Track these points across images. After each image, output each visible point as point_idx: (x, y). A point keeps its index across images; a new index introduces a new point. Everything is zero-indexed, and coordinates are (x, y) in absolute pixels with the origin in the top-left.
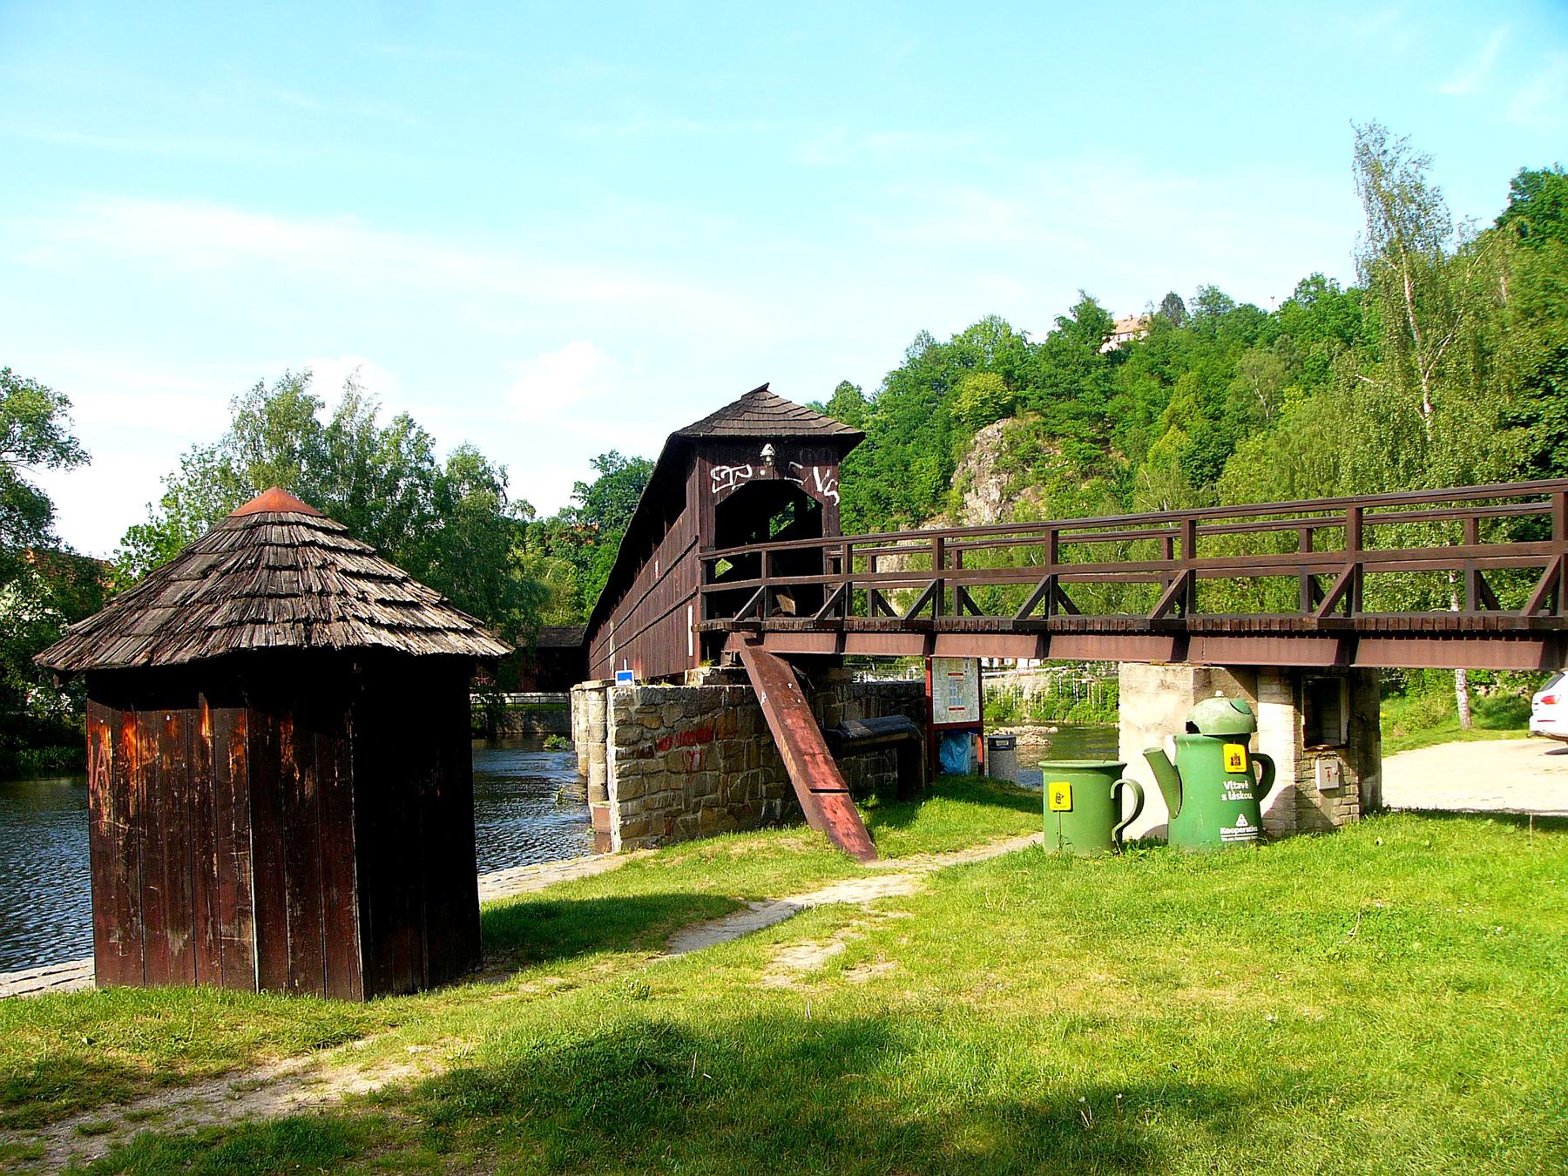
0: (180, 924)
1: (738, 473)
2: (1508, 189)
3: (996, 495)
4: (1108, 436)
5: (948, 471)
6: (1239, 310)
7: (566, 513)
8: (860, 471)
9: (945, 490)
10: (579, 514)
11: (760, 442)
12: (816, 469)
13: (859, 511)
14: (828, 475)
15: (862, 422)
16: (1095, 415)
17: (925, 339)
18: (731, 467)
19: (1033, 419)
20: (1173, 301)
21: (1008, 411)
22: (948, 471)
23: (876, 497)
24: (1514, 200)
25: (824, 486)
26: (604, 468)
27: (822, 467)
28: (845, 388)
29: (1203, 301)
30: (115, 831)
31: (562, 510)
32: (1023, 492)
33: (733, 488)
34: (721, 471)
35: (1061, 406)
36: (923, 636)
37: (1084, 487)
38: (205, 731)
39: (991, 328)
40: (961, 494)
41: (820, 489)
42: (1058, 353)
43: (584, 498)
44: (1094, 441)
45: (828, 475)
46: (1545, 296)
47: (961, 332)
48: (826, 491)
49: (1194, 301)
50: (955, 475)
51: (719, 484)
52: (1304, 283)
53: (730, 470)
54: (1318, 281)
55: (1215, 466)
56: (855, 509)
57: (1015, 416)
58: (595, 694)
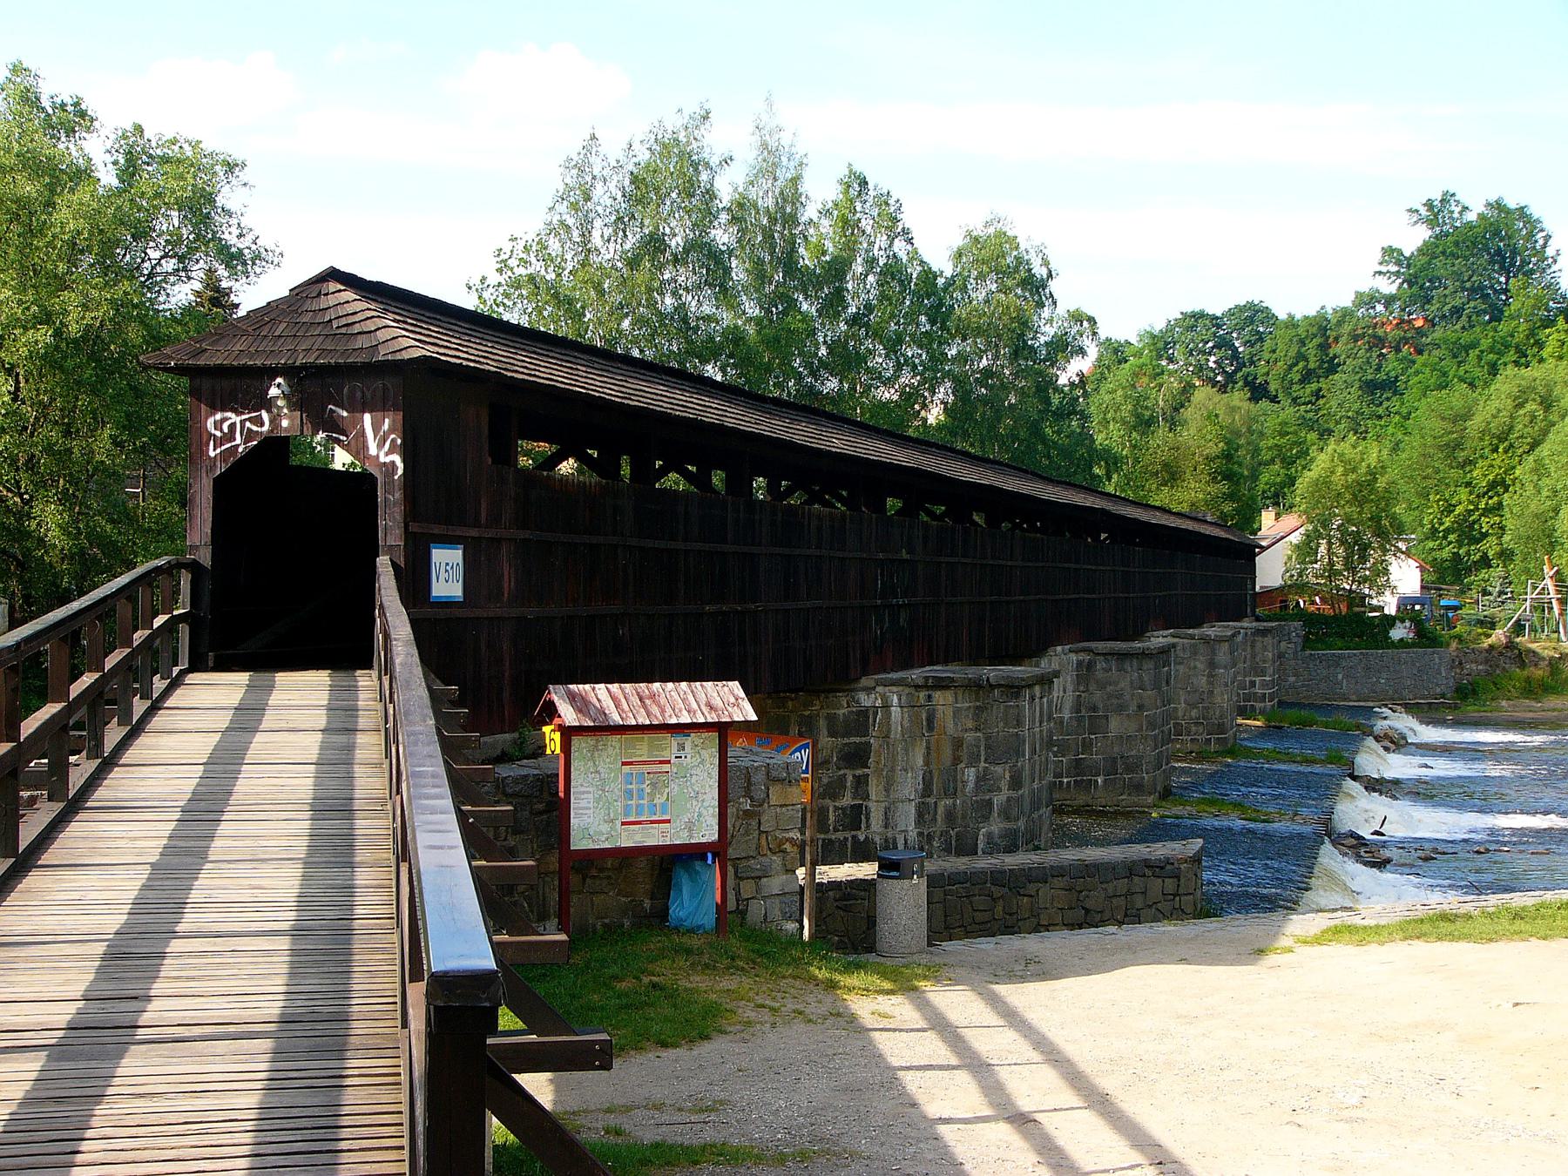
1: (248, 424)
7: (1367, 300)
10: (1389, 301)
12: (367, 417)
14: (386, 427)
18: (238, 413)
25: (380, 446)
26: (1432, 222)
27: (380, 414)
31: (1359, 295)
33: (240, 450)
34: (224, 420)
36: (578, 843)
41: (373, 450)
43: (1397, 274)
45: (386, 427)
48: (382, 455)
53: (234, 418)
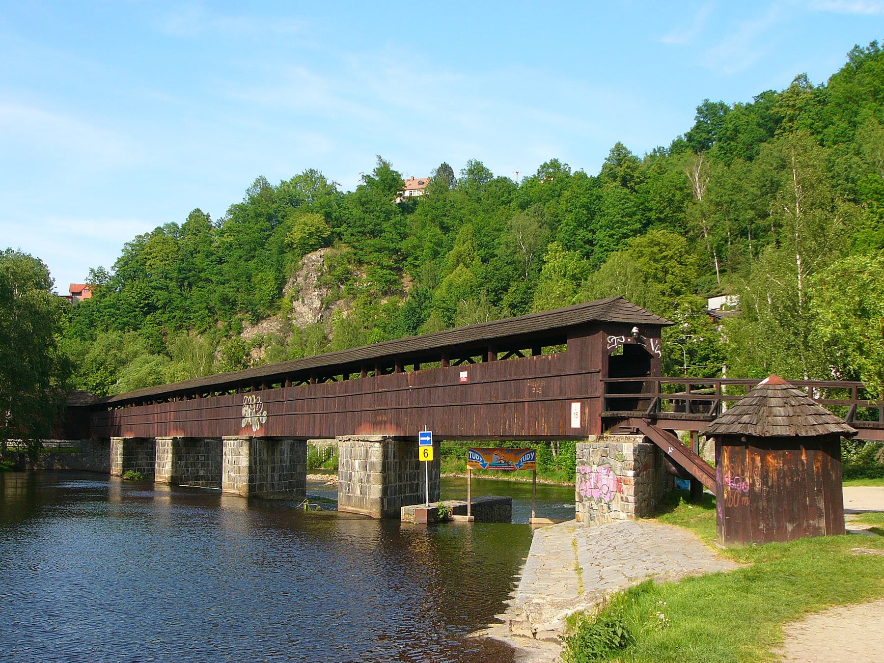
0: (792, 520)
2: (695, 113)
3: (317, 304)
4: (401, 266)
5: (281, 284)
6: (497, 181)
8: (213, 278)
9: (279, 298)
11: (632, 325)
12: (651, 340)
13: (210, 310)
15: (212, 242)
16: (392, 250)
17: (263, 185)
18: (616, 336)
19: (345, 249)
20: (445, 169)
21: (327, 243)
22: (281, 284)
23: (225, 300)
24: (699, 122)
28: (197, 215)
29: (471, 172)
30: (762, 490)
32: (338, 303)
35: (369, 242)
37: (384, 302)
38: (803, 457)
39: (311, 178)
40: (291, 301)
41: (653, 350)
42: (366, 203)
44: (392, 269)
46: (732, 195)
47: (288, 180)
49: (464, 172)
50: (286, 287)
51: (610, 345)
52: (545, 166)
53: (615, 338)
54: (555, 164)
55: (496, 295)
56: (207, 308)
57: (333, 246)
58: (377, 445)
